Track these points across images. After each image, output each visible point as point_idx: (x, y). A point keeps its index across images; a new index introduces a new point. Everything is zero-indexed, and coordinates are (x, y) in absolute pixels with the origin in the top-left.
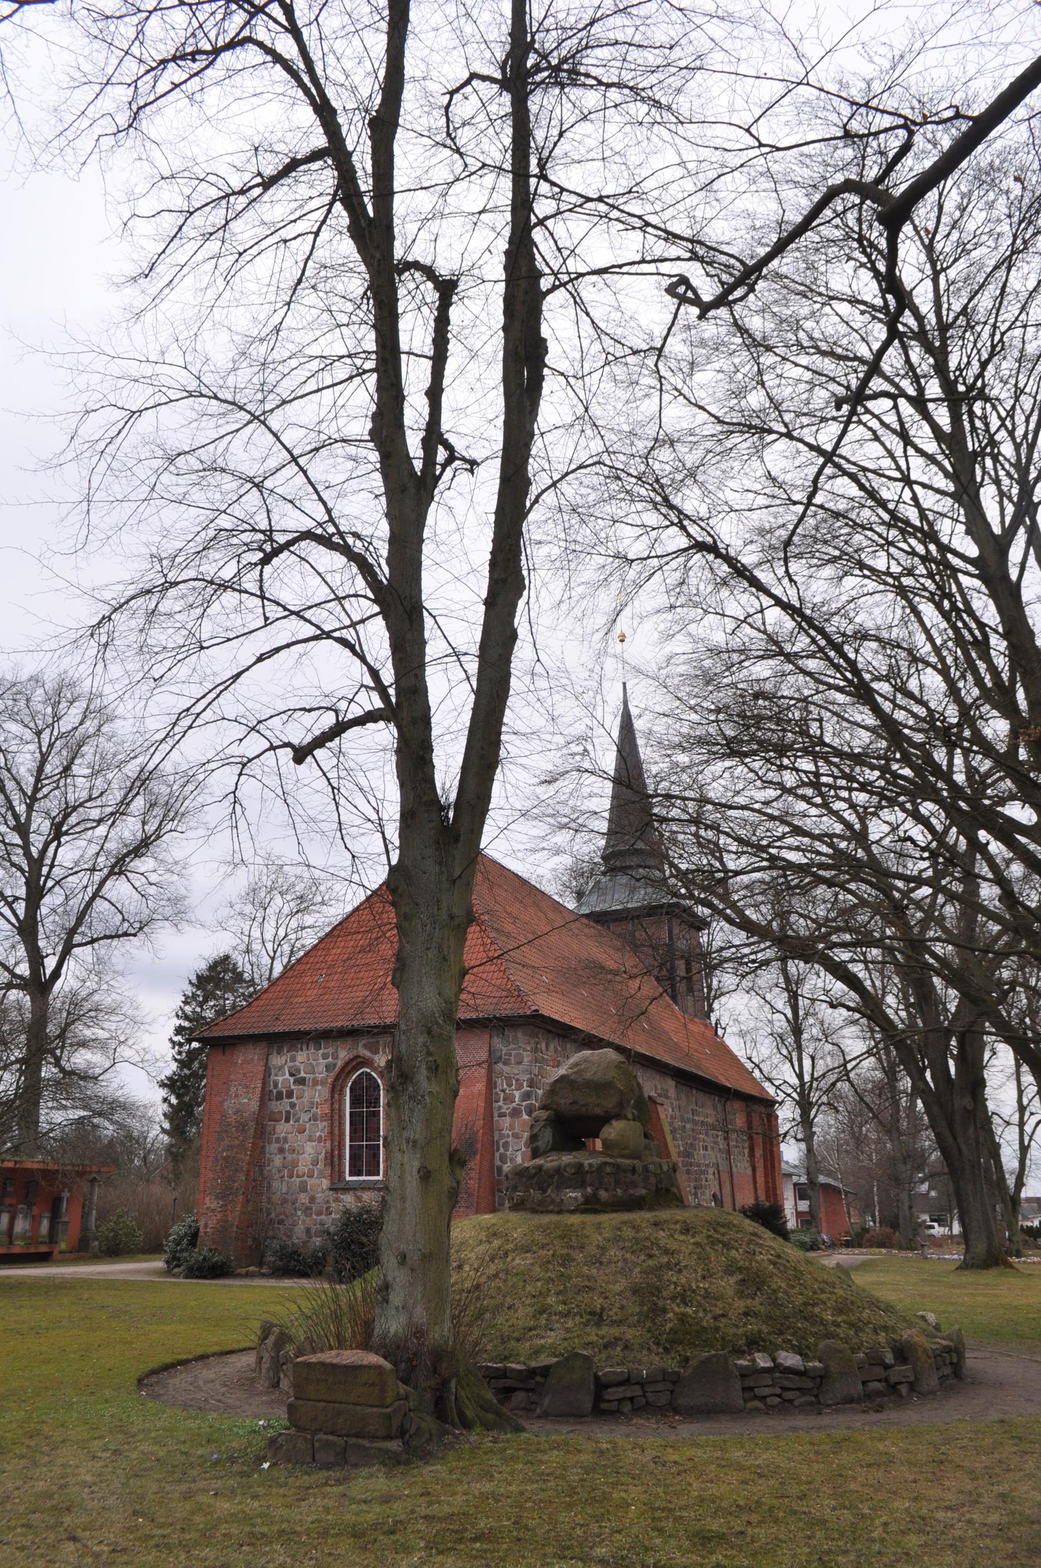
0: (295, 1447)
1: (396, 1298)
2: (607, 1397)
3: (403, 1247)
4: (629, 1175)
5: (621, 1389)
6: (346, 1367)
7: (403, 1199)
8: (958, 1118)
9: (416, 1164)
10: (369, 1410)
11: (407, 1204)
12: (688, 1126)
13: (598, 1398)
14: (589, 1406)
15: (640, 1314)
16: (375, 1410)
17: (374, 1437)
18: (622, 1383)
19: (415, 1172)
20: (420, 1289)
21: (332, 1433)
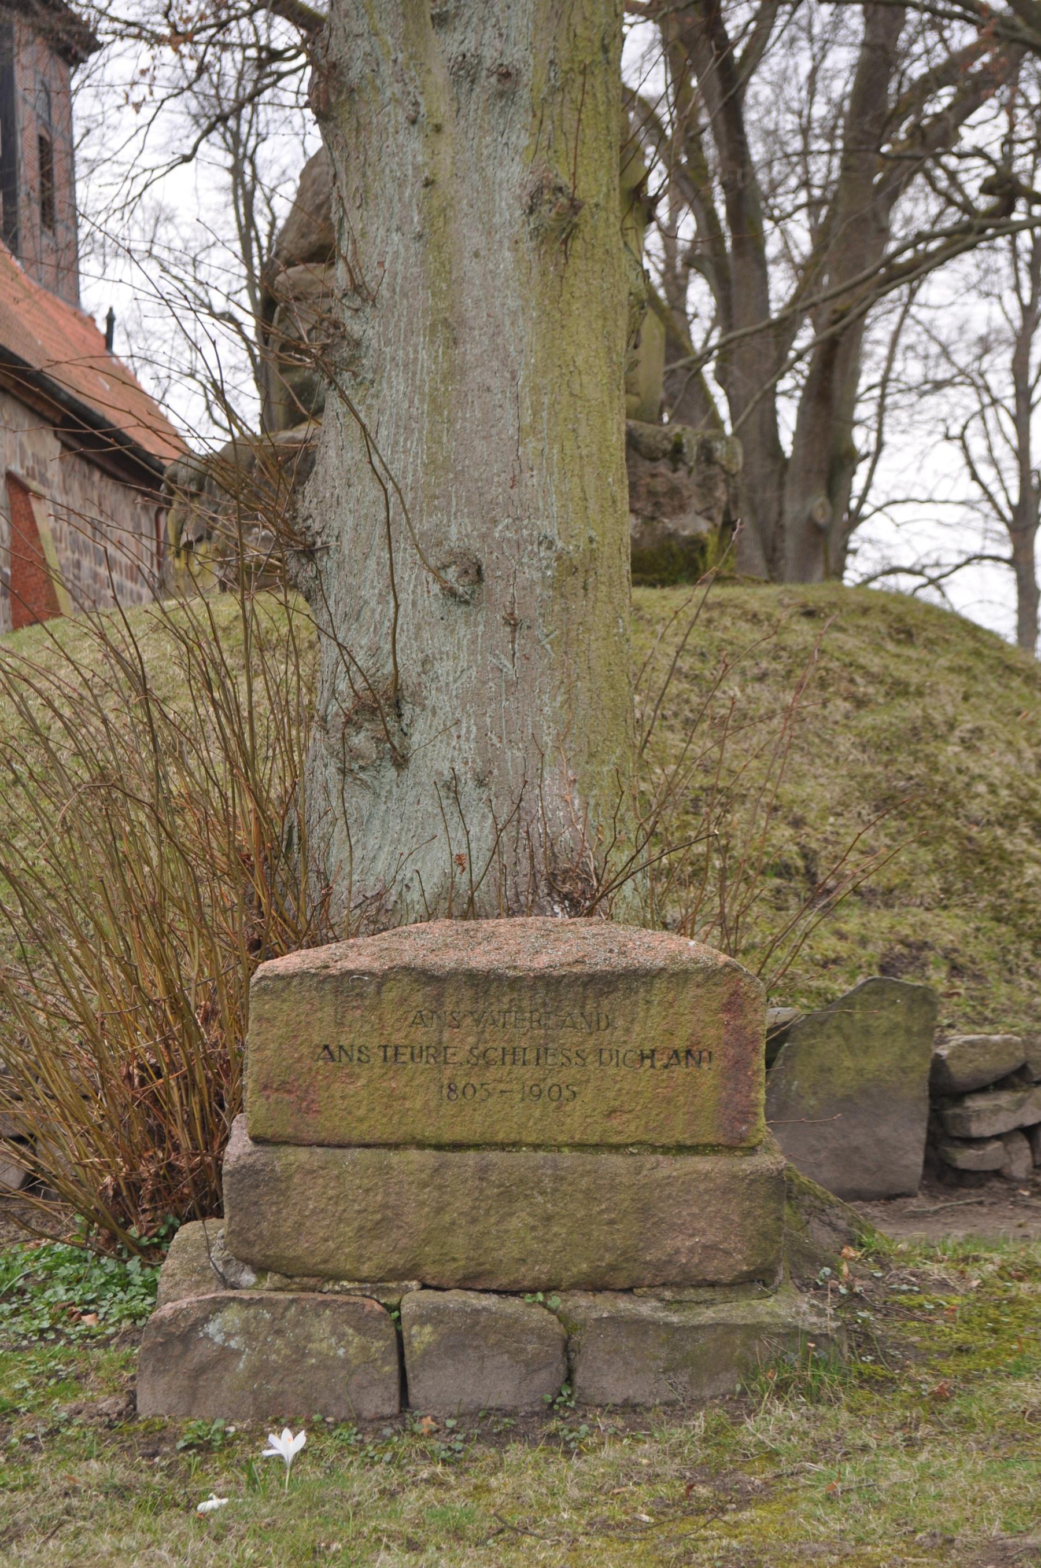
0: (300, 1353)
1: (440, 746)
2: (977, 1129)
3: (459, 531)
4: (663, 467)
5: (1005, 1098)
6: (548, 982)
7: (449, 330)
8: (790, 545)
9: (513, 176)
10: (670, 1167)
11: (471, 350)
12: (86, 563)
13: (943, 1134)
14: (915, 1159)
15: (940, 865)
16: (703, 1164)
17: (688, 1282)
18: (1002, 1083)
19: (508, 208)
20: (551, 704)
21: (466, 1284)
